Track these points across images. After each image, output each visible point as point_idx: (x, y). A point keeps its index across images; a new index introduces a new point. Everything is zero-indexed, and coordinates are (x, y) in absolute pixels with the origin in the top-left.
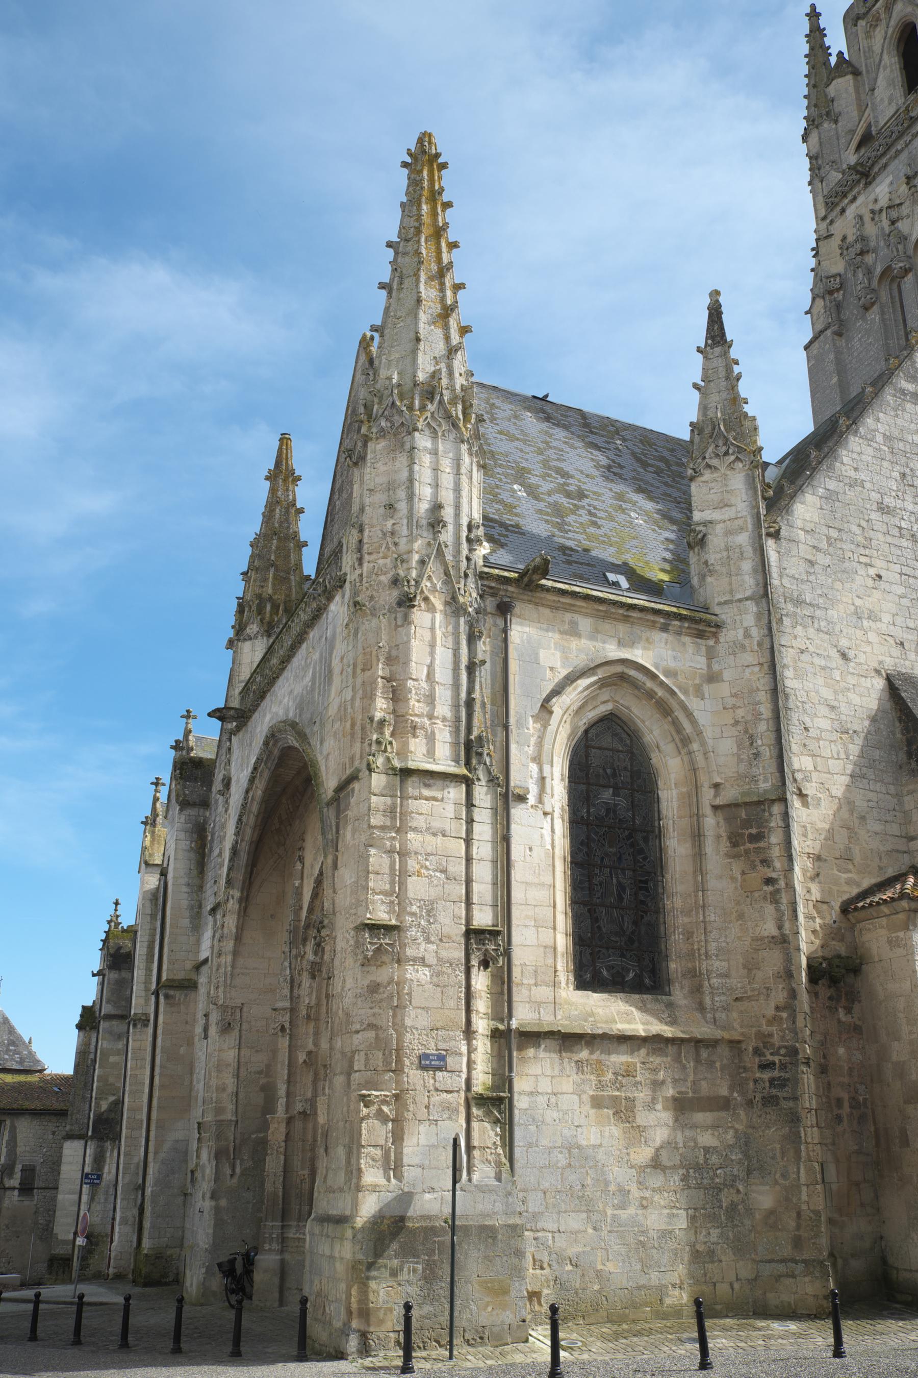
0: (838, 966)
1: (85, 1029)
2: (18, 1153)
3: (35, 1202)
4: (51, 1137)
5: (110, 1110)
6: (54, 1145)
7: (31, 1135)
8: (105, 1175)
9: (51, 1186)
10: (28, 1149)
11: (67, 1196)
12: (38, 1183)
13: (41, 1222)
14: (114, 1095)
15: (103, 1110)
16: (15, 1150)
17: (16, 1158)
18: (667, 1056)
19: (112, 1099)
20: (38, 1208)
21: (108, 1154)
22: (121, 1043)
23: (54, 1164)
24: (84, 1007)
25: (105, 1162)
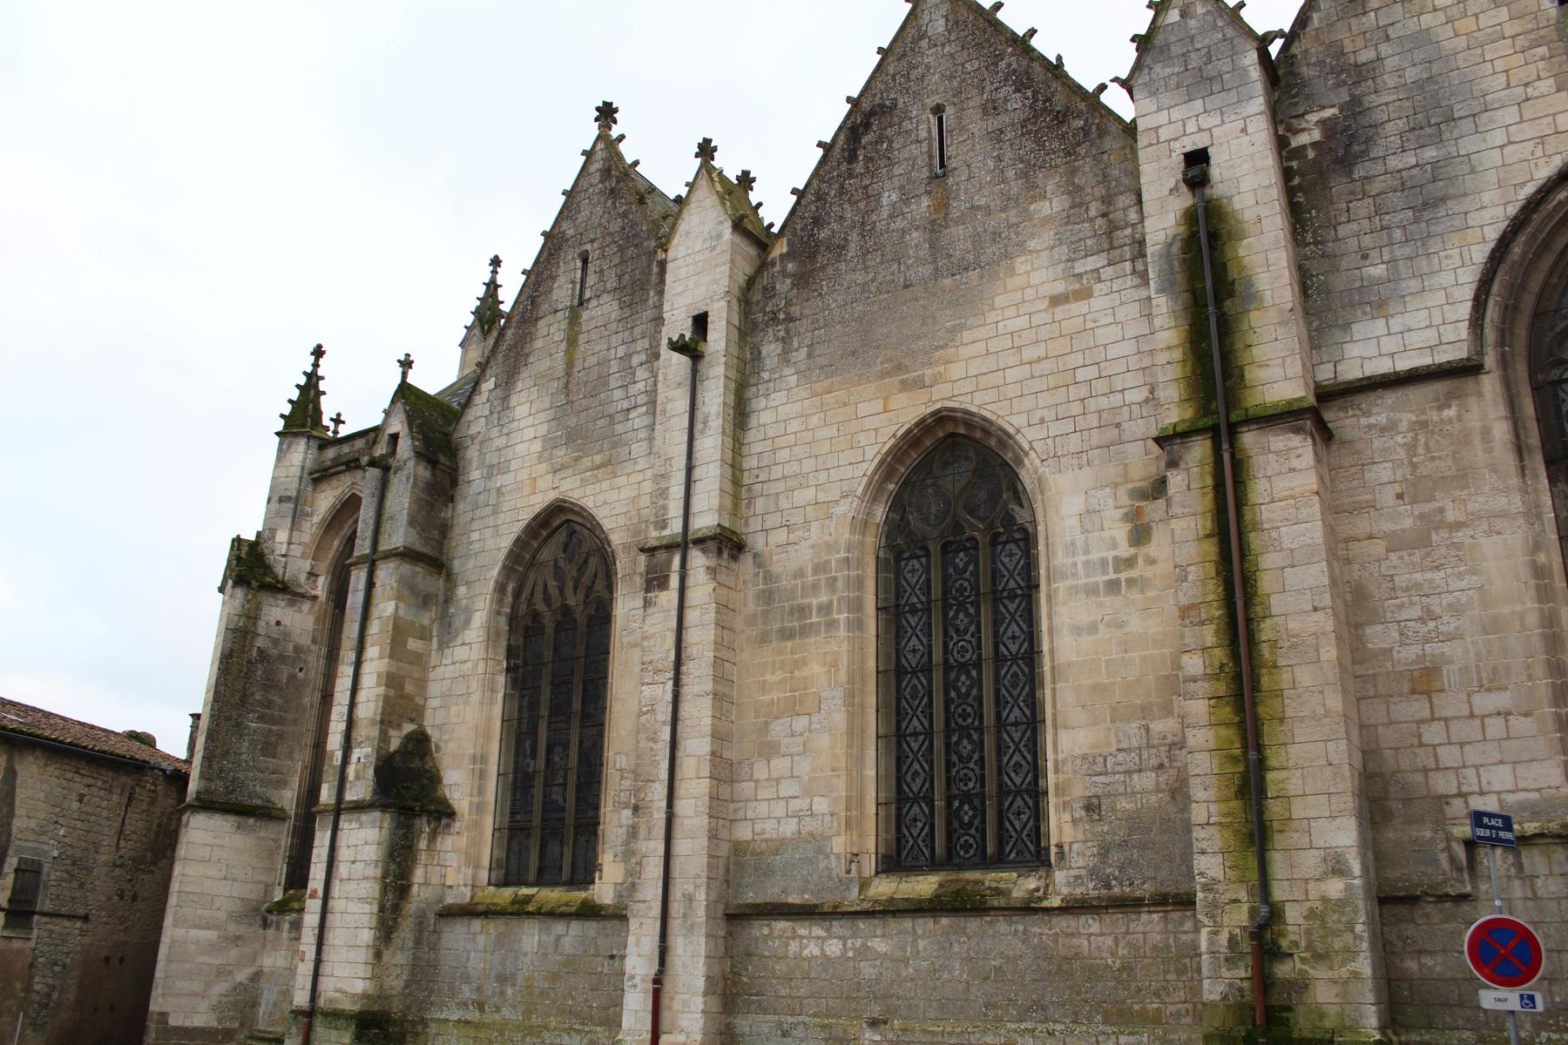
0: (620, 277)
1: (248, 584)
2: (14, 830)
3: (32, 944)
4: (75, 805)
5: (404, 751)
6: (79, 824)
7: (42, 795)
8: (415, 889)
9: (64, 910)
10: (33, 824)
11: (194, 933)
12: (44, 903)
13: (37, 987)
14: (412, 721)
15: (393, 748)
16: (9, 824)
17: (8, 841)
18: (1382, 1029)
19: (409, 728)
20: (35, 958)
21: (423, 844)
22: (427, 615)
23: (74, 863)
24: (238, 542)
25: (414, 861)
